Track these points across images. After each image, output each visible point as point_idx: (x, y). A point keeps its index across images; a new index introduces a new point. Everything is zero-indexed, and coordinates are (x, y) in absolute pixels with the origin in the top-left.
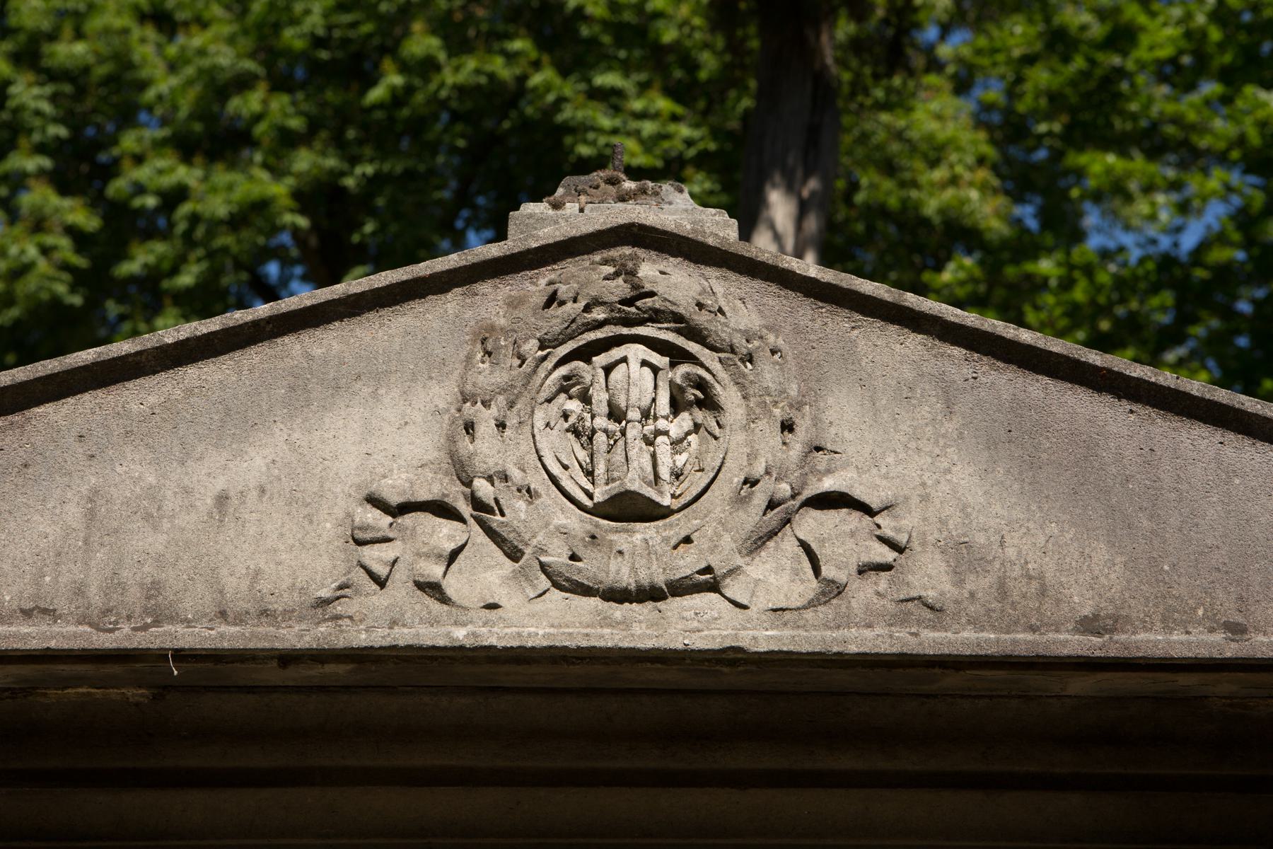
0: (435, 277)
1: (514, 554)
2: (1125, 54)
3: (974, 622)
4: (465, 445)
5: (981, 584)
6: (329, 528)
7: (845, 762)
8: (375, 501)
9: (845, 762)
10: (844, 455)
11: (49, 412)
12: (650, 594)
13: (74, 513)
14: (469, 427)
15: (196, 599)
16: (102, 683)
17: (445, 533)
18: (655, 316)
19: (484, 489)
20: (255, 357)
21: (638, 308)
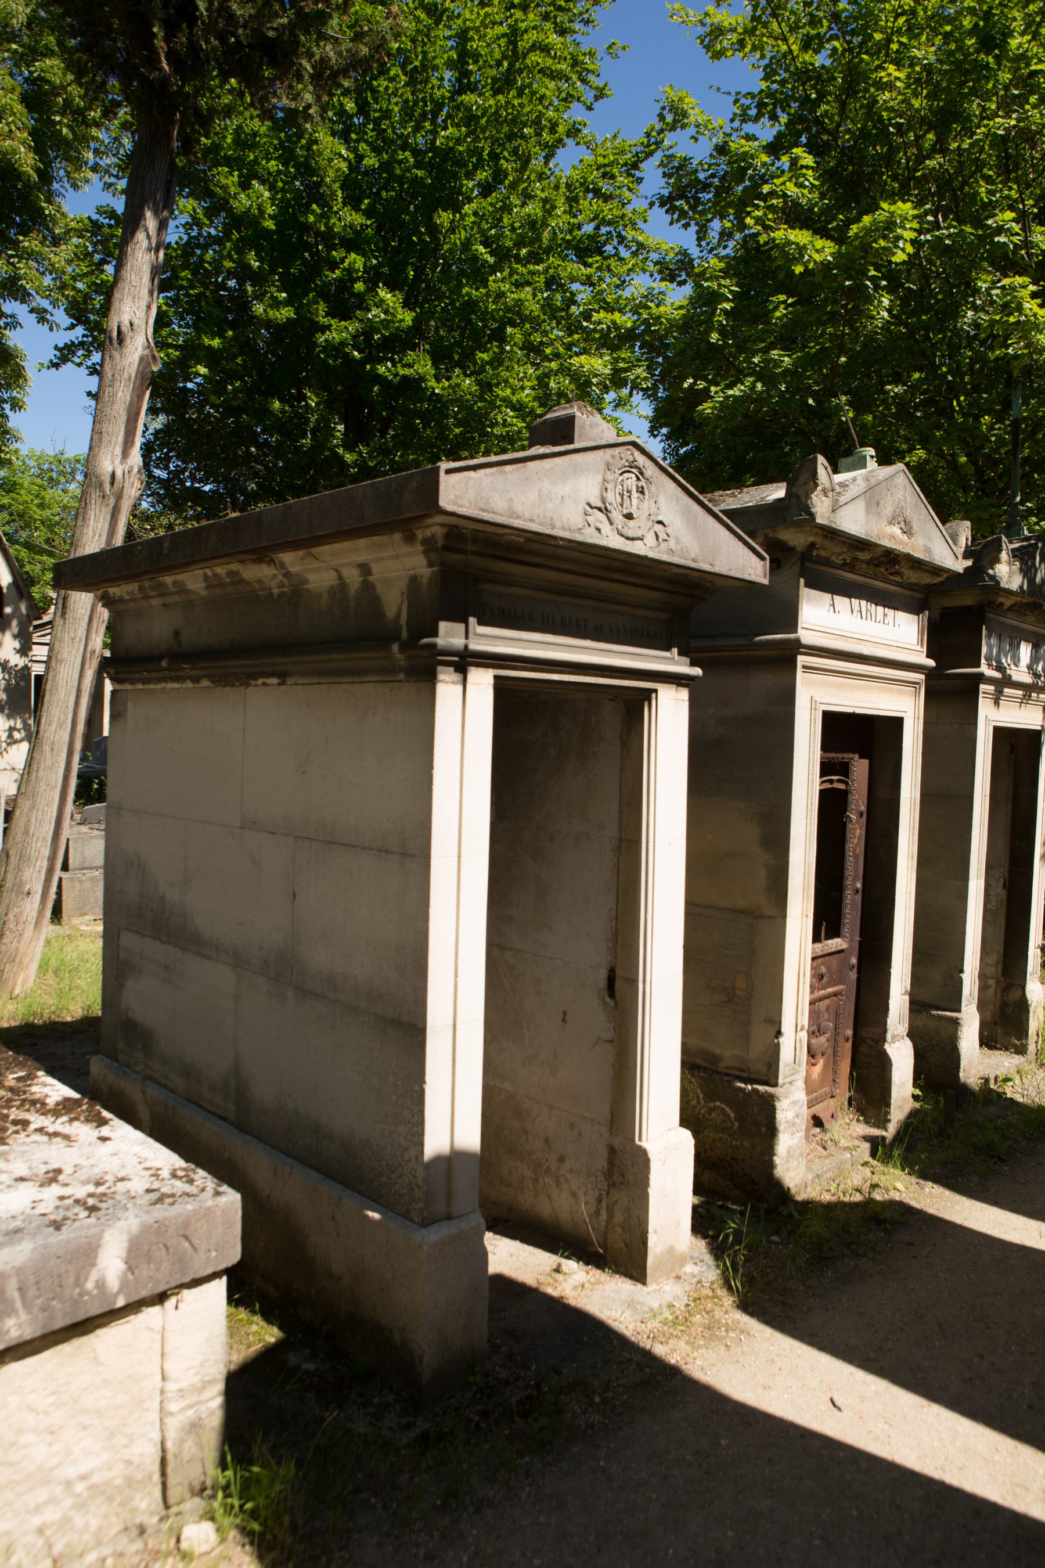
0: (866, 892)
1: (611, 524)
2: (768, 113)
3: (679, 556)
4: (605, 494)
5: (679, 547)
6: (581, 511)
7: (631, 580)
8: (589, 505)
9: (631, 580)
10: (552, 178)
11: (529, 464)
12: (633, 539)
13: (536, 494)
14: (606, 489)
15: (558, 524)
16: (517, 536)
17: (600, 514)
18: (636, 467)
19: (609, 507)
20: (567, 458)
21: (633, 454)
